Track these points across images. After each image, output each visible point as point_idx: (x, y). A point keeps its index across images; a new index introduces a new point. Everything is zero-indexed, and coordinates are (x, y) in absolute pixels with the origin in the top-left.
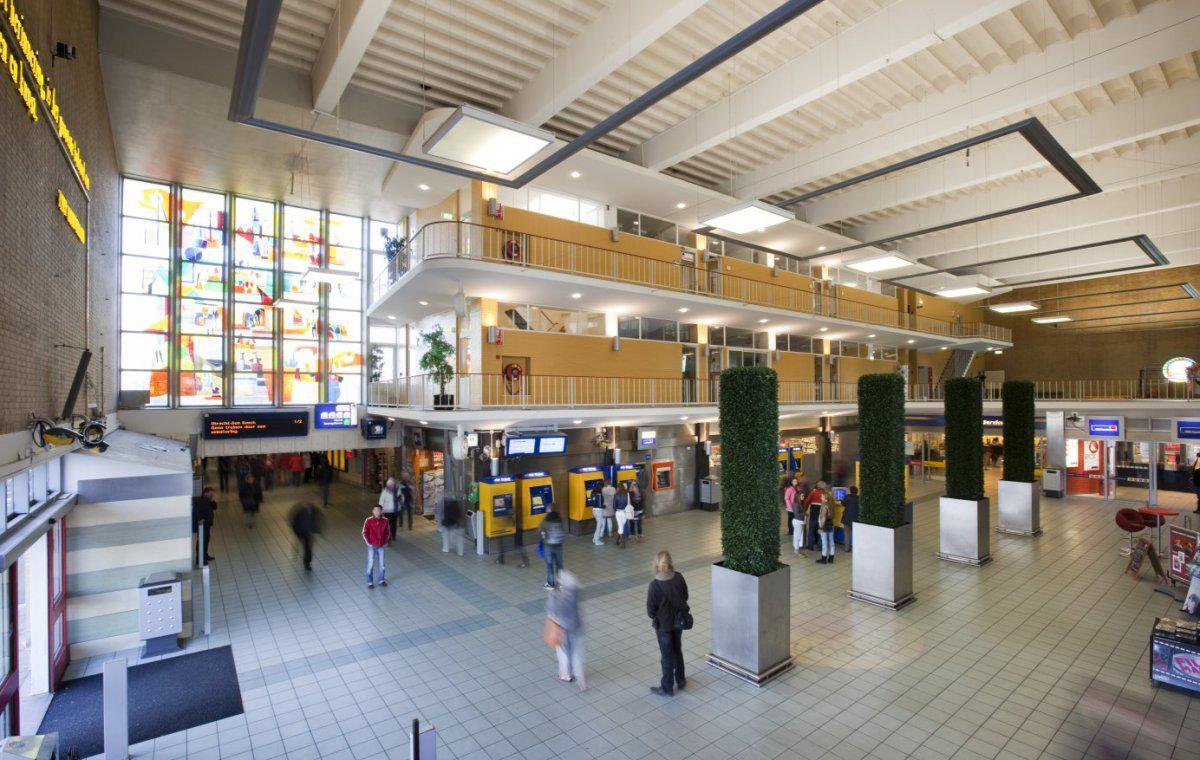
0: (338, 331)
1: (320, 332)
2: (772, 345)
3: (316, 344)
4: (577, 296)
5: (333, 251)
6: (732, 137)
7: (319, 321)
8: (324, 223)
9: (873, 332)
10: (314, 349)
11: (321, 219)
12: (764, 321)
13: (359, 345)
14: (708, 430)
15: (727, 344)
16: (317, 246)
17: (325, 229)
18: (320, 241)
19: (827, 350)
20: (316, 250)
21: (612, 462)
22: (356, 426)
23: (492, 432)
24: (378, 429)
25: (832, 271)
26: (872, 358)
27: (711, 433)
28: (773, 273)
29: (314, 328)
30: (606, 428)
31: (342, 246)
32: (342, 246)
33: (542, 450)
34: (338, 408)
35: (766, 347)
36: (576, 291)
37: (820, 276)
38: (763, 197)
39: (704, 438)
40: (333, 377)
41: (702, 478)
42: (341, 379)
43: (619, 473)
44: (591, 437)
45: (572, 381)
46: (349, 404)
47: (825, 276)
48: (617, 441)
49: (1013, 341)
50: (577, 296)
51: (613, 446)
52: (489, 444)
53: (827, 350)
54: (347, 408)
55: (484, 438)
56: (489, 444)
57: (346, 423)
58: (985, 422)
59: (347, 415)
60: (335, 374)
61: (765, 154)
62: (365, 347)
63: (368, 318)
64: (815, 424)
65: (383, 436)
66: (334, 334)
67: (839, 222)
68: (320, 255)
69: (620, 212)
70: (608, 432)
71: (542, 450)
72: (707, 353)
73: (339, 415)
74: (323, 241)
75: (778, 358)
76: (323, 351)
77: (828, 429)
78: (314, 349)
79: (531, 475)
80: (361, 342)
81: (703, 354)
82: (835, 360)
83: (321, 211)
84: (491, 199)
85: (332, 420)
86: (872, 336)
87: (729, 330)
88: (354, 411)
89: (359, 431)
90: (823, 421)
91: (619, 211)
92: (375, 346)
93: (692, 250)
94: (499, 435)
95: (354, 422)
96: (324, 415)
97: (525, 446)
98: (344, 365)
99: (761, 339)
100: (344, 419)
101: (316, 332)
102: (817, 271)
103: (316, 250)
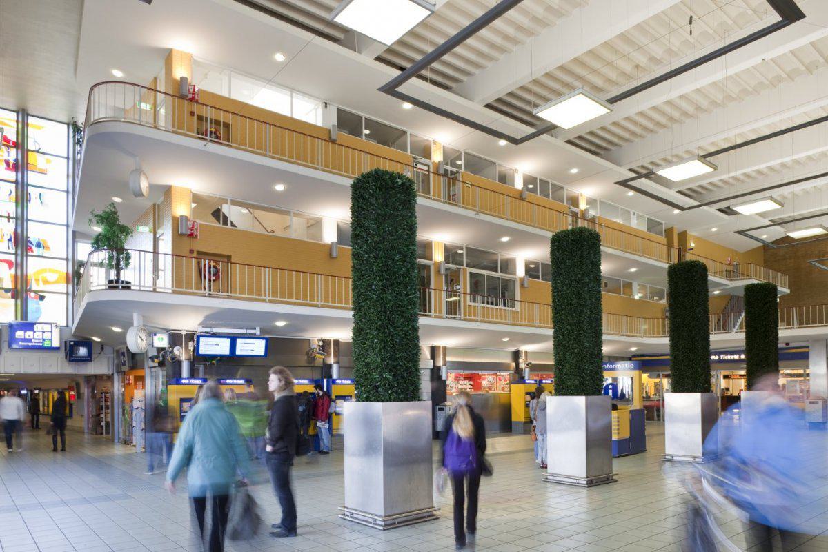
0: (39, 245)
1: (16, 244)
2: (521, 272)
3: (12, 258)
4: (280, 187)
5: (32, 158)
6: (534, 78)
7: (16, 233)
8: (20, 126)
9: (635, 263)
10: (10, 263)
11: (17, 121)
12: (505, 239)
13: (65, 262)
14: (445, 355)
15: (468, 265)
16: (13, 151)
17: (22, 132)
18: (16, 145)
20: (13, 155)
21: (329, 376)
22: (57, 349)
23: (184, 333)
24: (83, 351)
25: (591, 202)
27: (449, 359)
28: (520, 196)
29: (10, 240)
30: (323, 341)
31: (43, 153)
32: (43, 153)
33: (238, 352)
34: (36, 327)
35: (514, 274)
36: (505, 337)
37: (577, 206)
38: (490, 101)
39: (440, 363)
40: (33, 294)
41: (438, 405)
42: (42, 298)
43: (334, 387)
44: (306, 349)
45: (267, 272)
46: (51, 324)
47: (583, 206)
48: (335, 356)
49: (789, 288)
50: (280, 187)
51: (331, 360)
52: (181, 346)
54: (48, 328)
55: (175, 338)
56: (181, 346)
57: (47, 344)
58: (743, 357)
59: (47, 336)
60: (35, 292)
61: (633, 133)
62: (70, 264)
63: (74, 232)
65: (88, 359)
66: (34, 248)
68: (17, 160)
69: (340, 112)
70: (325, 344)
71: (238, 352)
72: (443, 271)
73: (38, 335)
74: (20, 145)
75: (526, 285)
76: (19, 265)
78: (10, 263)
79: (229, 381)
80: (67, 259)
81: (438, 272)
83: (17, 112)
84: (182, 78)
85: (30, 340)
86: (633, 270)
87: (470, 251)
88: (56, 333)
89: (62, 354)
91: (339, 110)
92: (82, 264)
93: (424, 160)
94: (190, 336)
95: (56, 344)
96: (19, 334)
97: (220, 347)
98: (46, 282)
99: (507, 266)
100: (44, 340)
101: (12, 244)
102: (574, 201)
103: (13, 155)
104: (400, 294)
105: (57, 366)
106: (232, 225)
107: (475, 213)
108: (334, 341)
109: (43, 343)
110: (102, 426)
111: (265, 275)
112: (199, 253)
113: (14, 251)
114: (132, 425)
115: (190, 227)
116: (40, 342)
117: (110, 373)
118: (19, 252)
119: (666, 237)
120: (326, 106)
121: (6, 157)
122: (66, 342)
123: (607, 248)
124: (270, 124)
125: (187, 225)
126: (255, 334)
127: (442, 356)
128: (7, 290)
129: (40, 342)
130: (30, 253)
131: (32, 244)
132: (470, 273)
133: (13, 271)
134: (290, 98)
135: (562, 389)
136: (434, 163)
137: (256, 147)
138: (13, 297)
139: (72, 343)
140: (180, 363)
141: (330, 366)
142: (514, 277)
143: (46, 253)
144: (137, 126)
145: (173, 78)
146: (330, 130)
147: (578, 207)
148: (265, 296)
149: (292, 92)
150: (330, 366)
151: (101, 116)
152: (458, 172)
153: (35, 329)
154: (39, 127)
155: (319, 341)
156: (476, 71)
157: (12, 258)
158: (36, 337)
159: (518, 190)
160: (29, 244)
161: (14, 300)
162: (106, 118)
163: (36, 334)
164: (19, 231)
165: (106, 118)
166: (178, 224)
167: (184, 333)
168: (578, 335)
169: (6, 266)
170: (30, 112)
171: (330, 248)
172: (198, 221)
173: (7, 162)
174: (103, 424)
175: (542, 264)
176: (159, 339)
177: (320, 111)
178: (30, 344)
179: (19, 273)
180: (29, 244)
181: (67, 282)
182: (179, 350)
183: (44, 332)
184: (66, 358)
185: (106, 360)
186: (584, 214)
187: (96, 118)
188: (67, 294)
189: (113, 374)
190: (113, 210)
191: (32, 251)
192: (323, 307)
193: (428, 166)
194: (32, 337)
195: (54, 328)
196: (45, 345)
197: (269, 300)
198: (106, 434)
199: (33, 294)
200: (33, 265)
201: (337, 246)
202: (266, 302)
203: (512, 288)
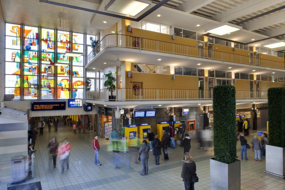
1: (69, 74)
2: (233, 77)
3: (68, 78)
4: (160, 60)
7: (69, 70)
8: (71, 36)
12: (230, 68)
14: (208, 109)
15: (216, 77)
17: (71, 38)
19: (255, 79)
23: (129, 109)
24: (89, 108)
25: (257, 48)
26: (274, 81)
27: (210, 110)
28: (233, 49)
34: (76, 100)
37: (253, 51)
39: (207, 112)
41: (206, 126)
47: (255, 50)
50: (160, 60)
53: (255, 79)
54: (79, 100)
55: (126, 111)
57: (79, 105)
60: (75, 88)
64: (250, 107)
65: (91, 110)
67: (260, 29)
68: (69, 47)
75: (235, 82)
77: (256, 109)
81: (206, 80)
82: (258, 82)
85: (74, 105)
86: (273, 73)
88: (81, 101)
89: (83, 108)
90: (254, 106)
93: (202, 42)
94: (132, 110)
95: (81, 105)
96: (71, 103)
97: (141, 114)
100: (78, 104)
102: (251, 48)
104: (232, 127)
105: (82, 112)
106: (143, 72)
107: (222, 61)
108: (174, 107)
109: (77, 105)
110: (90, 128)
111: (157, 91)
112: (133, 82)
113: (69, 76)
114: (105, 132)
115: (131, 74)
116: (76, 105)
117: (97, 114)
118: (70, 76)
119: (284, 58)
120: (171, 28)
121: (66, 47)
122: (84, 104)
123: (267, 68)
124: (158, 41)
125: (130, 74)
126: (151, 109)
127: (207, 109)
128: (67, 89)
129: (76, 105)
130: (73, 76)
131: (74, 73)
132: (217, 80)
133: (69, 82)
134: (160, 26)
135: (272, 143)
136: (205, 42)
137: (153, 48)
138: (69, 91)
139: (87, 106)
140: (128, 119)
141: (172, 116)
142: (231, 79)
143: (78, 76)
144: (120, 48)
145: (125, 26)
146: (172, 36)
147: (253, 51)
148: (157, 99)
149: (160, 24)
150: (172, 116)
151: (109, 45)
152: (213, 44)
153: (75, 101)
154: (76, 36)
155: (169, 108)
156: (223, 12)
157: (68, 78)
158: (75, 104)
159: (233, 48)
160: (73, 73)
161: (69, 92)
162: (111, 46)
163: (76, 102)
164: (70, 69)
165: (111, 46)
166: (128, 73)
167: (129, 109)
168: (280, 126)
169: (67, 81)
170: (73, 31)
171: (173, 75)
172: (133, 72)
173: (67, 48)
174: (90, 127)
175: (240, 73)
176: (121, 111)
177: (169, 29)
178: (74, 106)
179: (70, 83)
180: (73, 73)
181: (84, 85)
182: (128, 115)
183: (78, 102)
184: (84, 110)
185: (95, 109)
186: (255, 53)
187: (108, 45)
188: (84, 88)
189: (97, 114)
190: (110, 73)
191: (74, 76)
192: (175, 100)
193: (203, 43)
194: (74, 104)
195: (80, 100)
196: (78, 106)
197: (188, 99)
198: (91, 130)
199: (74, 89)
200: (74, 80)
201: (175, 75)
202: (158, 101)
203: (230, 83)
